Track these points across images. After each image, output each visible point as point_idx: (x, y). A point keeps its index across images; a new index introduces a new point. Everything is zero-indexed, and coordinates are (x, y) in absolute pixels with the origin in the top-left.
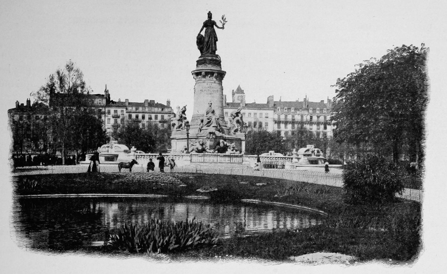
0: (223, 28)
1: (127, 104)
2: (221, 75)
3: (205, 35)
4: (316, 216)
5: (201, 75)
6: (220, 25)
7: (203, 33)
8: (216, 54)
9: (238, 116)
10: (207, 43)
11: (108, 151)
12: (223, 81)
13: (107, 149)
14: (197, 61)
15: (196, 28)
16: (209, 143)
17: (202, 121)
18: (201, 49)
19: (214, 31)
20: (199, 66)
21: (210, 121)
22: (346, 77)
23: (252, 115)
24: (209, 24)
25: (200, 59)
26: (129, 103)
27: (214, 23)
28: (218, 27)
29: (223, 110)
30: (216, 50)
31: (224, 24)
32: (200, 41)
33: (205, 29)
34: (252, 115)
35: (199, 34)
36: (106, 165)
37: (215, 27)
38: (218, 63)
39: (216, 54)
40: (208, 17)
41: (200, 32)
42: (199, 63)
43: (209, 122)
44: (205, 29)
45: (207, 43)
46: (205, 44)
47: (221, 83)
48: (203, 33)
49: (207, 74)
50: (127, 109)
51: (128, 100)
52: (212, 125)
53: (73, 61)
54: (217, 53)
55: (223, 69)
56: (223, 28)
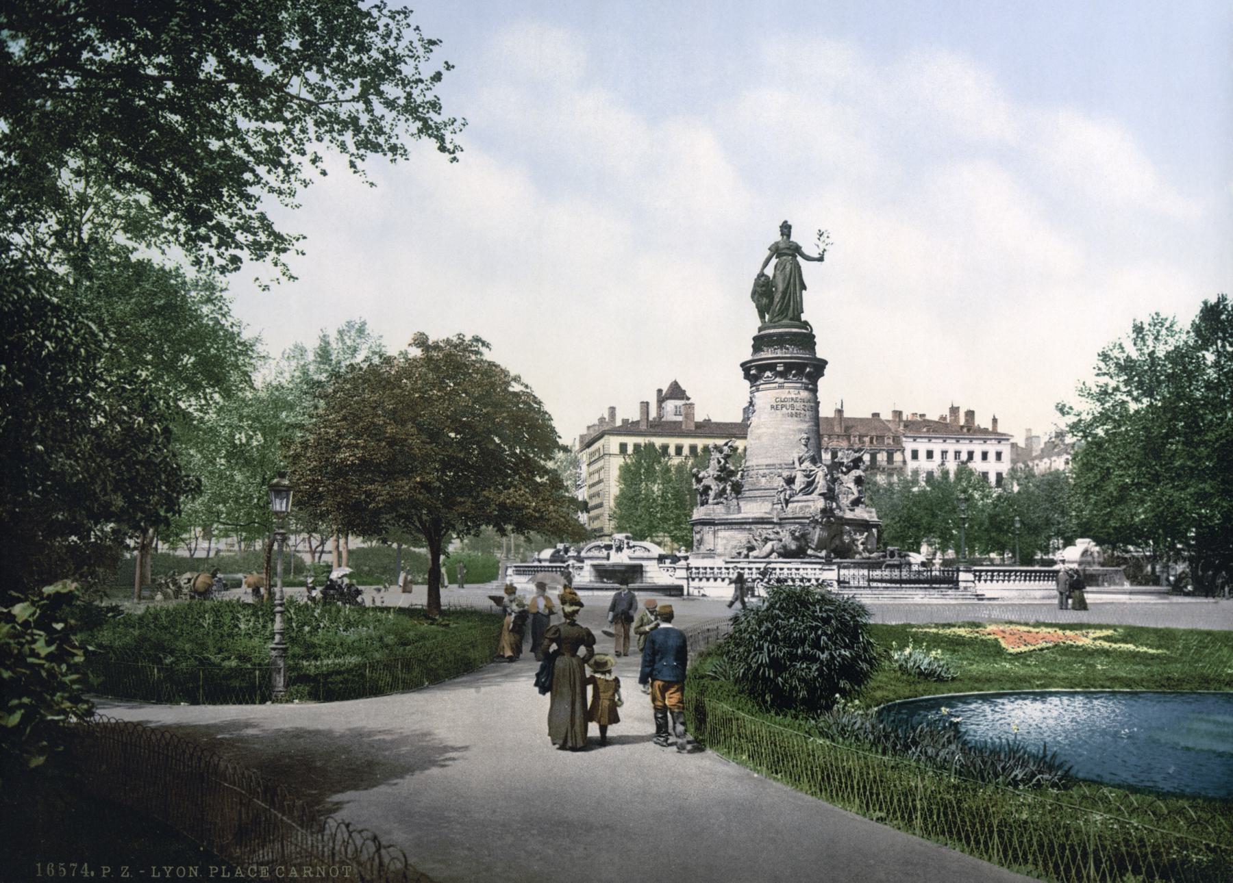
0: (821, 259)
2: (819, 367)
7: (770, 271)
10: (779, 296)
11: (608, 558)
12: (821, 382)
13: (605, 553)
15: (754, 260)
16: (816, 534)
17: (790, 481)
19: (798, 268)
21: (813, 481)
22: (347, 157)
23: (937, 457)
24: (786, 250)
26: (908, 425)
27: (796, 250)
32: (763, 292)
33: (774, 261)
34: (937, 457)
35: (762, 275)
36: (596, 593)
37: (799, 258)
38: (807, 340)
42: (760, 343)
43: (810, 484)
44: (774, 261)
45: (779, 296)
47: (814, 391)
48: (770, 271)
49: (789, 367)
52: (817, 491)
53: (264, 336)
54: (804, 317)
55: (819, 355)
56: (821, 259)
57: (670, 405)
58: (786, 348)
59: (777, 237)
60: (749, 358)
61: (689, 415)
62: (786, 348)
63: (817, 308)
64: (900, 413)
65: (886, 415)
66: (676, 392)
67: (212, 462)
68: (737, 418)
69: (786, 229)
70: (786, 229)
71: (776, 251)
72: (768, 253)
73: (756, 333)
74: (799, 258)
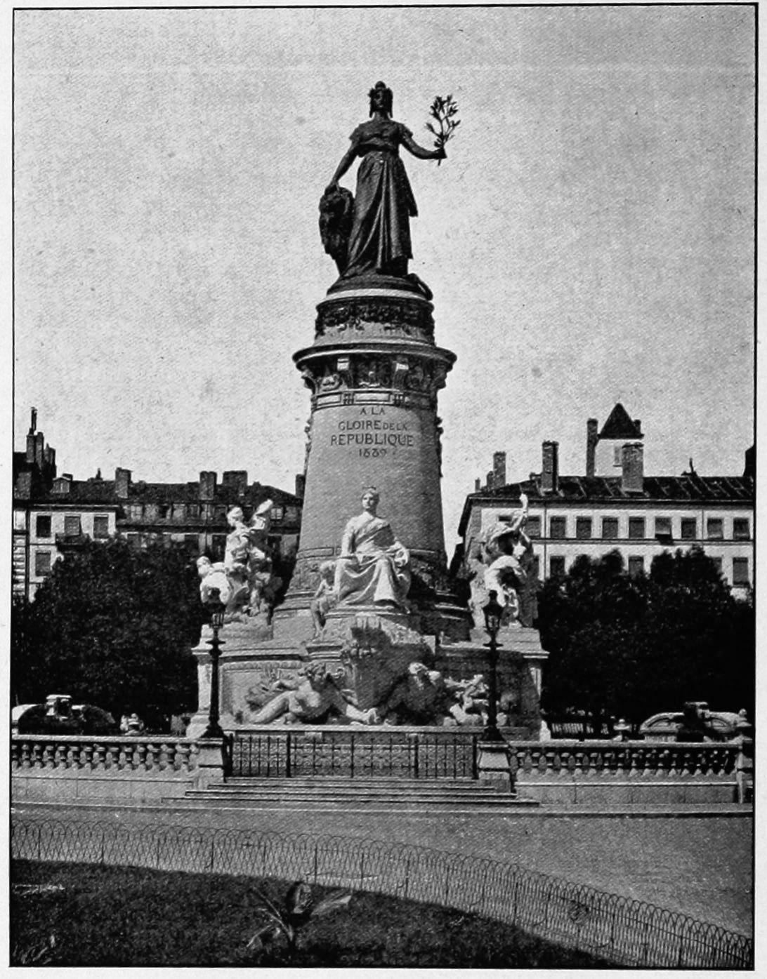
0: (440, 155)
1: (122, 493)
3: (358, 191)
4: (671, 956)
5: (333, 370)
6: (426, 141)
7: (349, 182)
8: (410, 272)
9: (509, 551)
14: (323, 308)
15: (317, 151)
18: (337, 251)
20: (327, 330)
24: (380, 140)
25: (334, 296)
27: (401, 135)
28: (421, 154)
29: (568, 539)
30: (407, 253)
31: (443, 137)
32: (336, 217)
35: (332, 189)
37: (403, 152)
38: (416, 312)
39: (410, 272)
40: (374, 108)
41: (342, 171)
42: (327, 314)
44: (358, 161)
46: (356, 230)
48: (349, 182)
50: (120, 515)
51: (128, 473)
56: (440, 155)
57: (609, 447)
58: (378, 330)
59: (363, 114)
60: (309, 342)
61: (631, 460)
62: (378, 330)
63: (437, 246)
64: (128, 473)
65: (109, 476)
66: (621, 425)
67: (89, 492)
68: (739, 470)
69: (381, 99)
70: (381, 99)
71: (360, 144)
72: (347, 145)
73: (323, 297)
74: (403, 152)
